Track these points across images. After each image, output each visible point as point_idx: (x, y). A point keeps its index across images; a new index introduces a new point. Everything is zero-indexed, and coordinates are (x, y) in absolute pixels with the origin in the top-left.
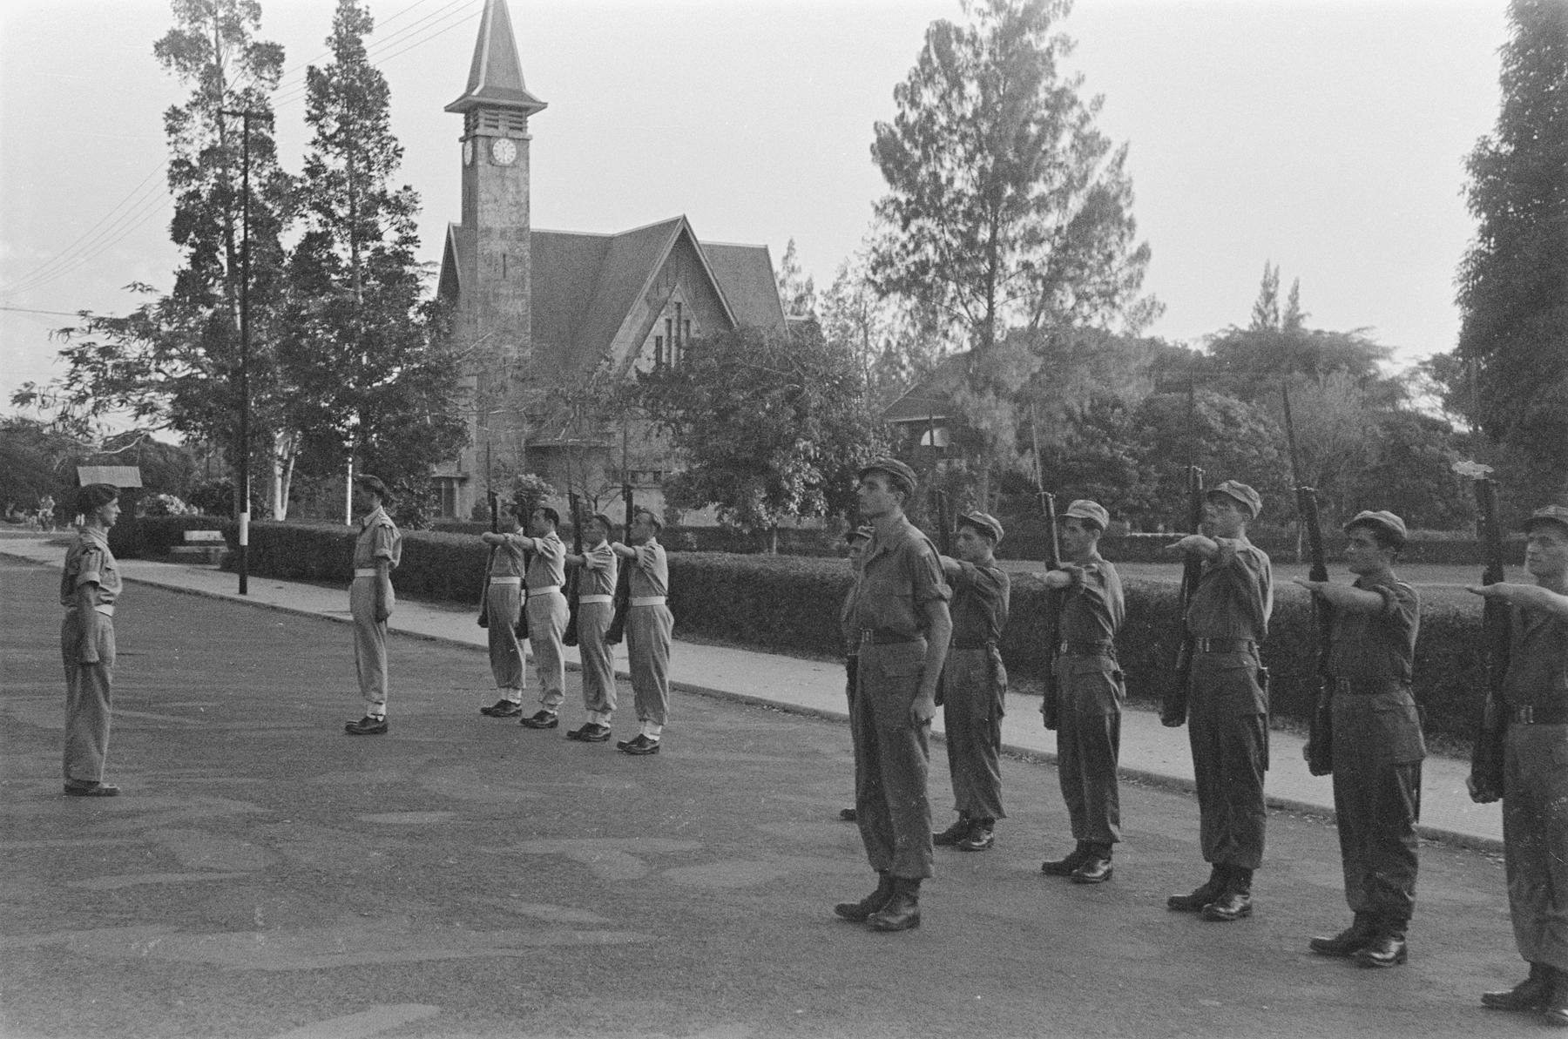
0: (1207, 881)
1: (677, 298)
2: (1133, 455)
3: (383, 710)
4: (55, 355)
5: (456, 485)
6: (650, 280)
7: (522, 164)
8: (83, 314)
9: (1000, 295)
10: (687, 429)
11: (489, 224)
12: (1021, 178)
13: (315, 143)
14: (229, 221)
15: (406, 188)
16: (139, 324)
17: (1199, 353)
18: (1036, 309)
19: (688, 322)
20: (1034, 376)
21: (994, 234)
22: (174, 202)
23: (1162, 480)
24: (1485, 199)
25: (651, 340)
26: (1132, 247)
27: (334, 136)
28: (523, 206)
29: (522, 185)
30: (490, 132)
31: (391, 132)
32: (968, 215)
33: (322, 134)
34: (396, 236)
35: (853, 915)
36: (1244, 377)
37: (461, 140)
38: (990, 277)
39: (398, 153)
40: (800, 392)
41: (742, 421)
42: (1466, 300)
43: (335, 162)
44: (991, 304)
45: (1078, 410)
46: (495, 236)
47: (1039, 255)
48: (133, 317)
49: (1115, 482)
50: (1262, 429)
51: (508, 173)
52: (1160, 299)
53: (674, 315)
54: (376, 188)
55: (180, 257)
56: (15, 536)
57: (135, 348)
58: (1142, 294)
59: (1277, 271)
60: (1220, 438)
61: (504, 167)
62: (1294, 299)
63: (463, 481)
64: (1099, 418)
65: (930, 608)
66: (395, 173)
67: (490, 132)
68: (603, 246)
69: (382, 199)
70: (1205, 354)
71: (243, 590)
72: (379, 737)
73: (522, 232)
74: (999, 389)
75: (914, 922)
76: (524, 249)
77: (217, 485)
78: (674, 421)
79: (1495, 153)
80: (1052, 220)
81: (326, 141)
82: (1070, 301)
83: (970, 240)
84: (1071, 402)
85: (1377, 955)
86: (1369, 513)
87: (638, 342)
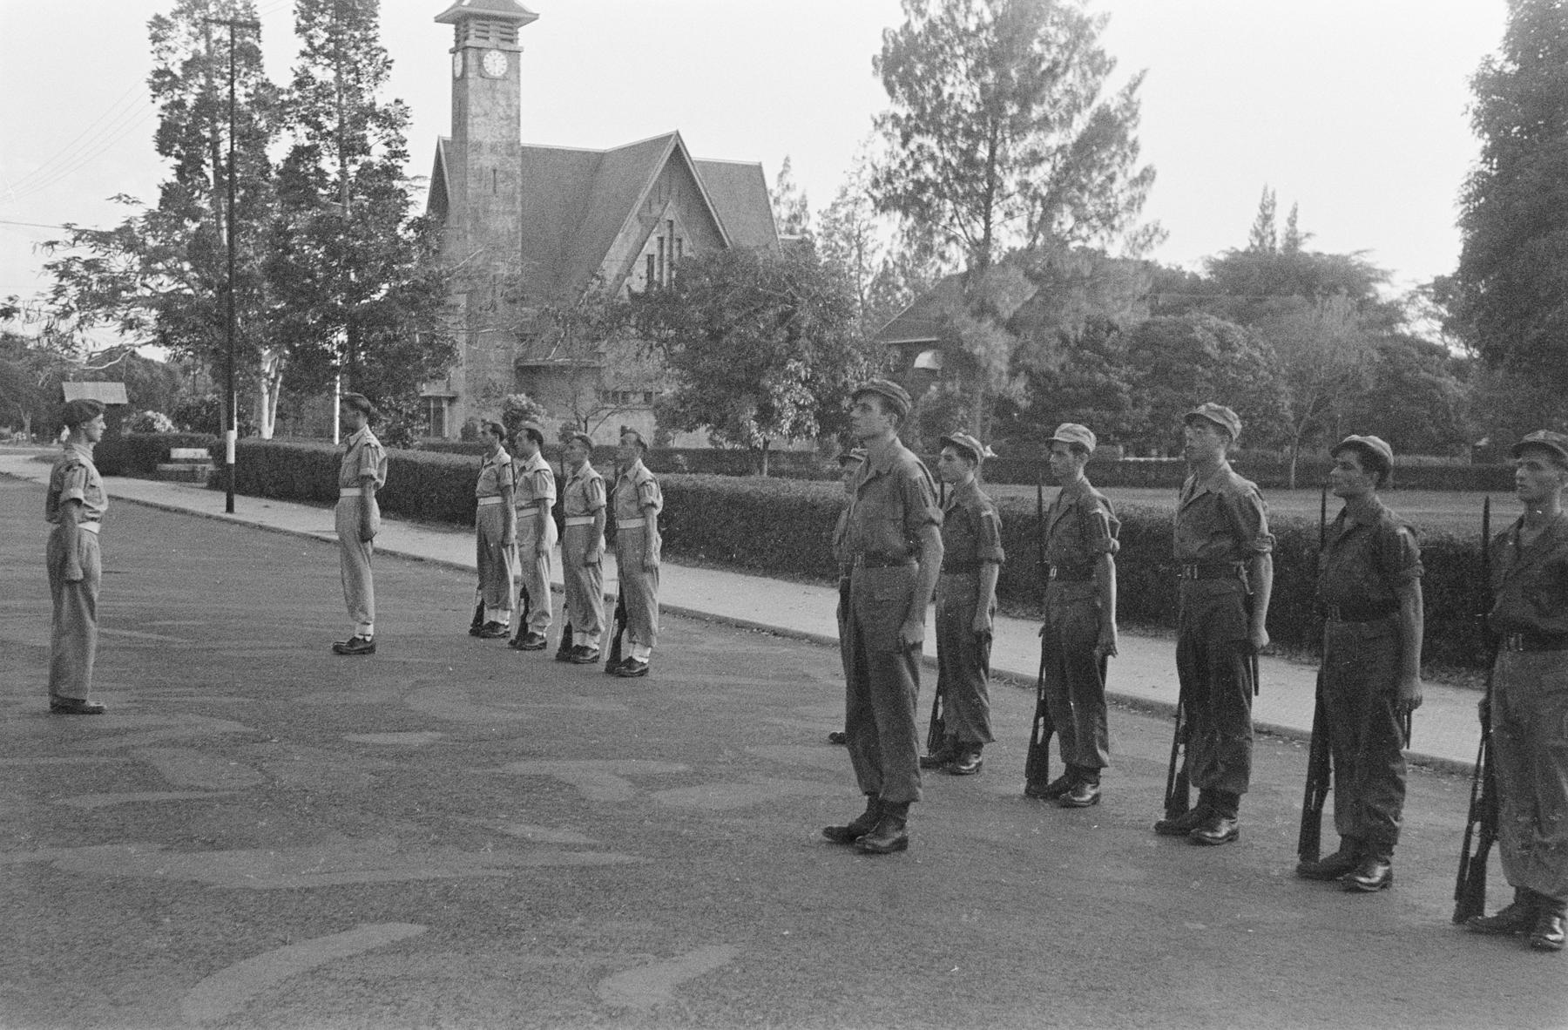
1: (669, 215)
3: (370, 630)
4: (40, 269)
5: (445, 405)
6: (642, 197)
8: (68, 226)
9: (997, 215)
10: (679, 348)
11: (479, 138)
12: (1026, 97)
14: (215, 132)
16: (126, 238)
19: (680, 240)
24: (1490, 119)
25: (642, 258)
26: (1135, 170)
27: (323, 47)
28: (514, 120)
29: (512, 97)
30: (480, 43)
33: (311, 45)
34: (385, 150)
37: (453, 52)
38: (988, 198)
39: (387, 64)
43: (323, 73)
44: (988, 223)
46: (486, 150)
47: (1040, 175)
49: (1109, 406)
50: (1257, 354)
51: (499, 86)
52: (1164, 226)
53: (666, 233)
55: (165, 170)
57: (121, 262)
61: (494, 80)
63: (452, 400)
64: (1093, 344)
67: (480, 43)
68: (594, 162)
69: (370, 113)
71: (230, 508)
73: (513, 147)
75: (901, 845)
76: (515, 166)
78: (666, 341)
81: (312, 53)
82: (1069, 222)
83: (968, 158)
84: (1067, 327)
85: (1363, 880)
86: (1356, 437)
87: (630, 261)
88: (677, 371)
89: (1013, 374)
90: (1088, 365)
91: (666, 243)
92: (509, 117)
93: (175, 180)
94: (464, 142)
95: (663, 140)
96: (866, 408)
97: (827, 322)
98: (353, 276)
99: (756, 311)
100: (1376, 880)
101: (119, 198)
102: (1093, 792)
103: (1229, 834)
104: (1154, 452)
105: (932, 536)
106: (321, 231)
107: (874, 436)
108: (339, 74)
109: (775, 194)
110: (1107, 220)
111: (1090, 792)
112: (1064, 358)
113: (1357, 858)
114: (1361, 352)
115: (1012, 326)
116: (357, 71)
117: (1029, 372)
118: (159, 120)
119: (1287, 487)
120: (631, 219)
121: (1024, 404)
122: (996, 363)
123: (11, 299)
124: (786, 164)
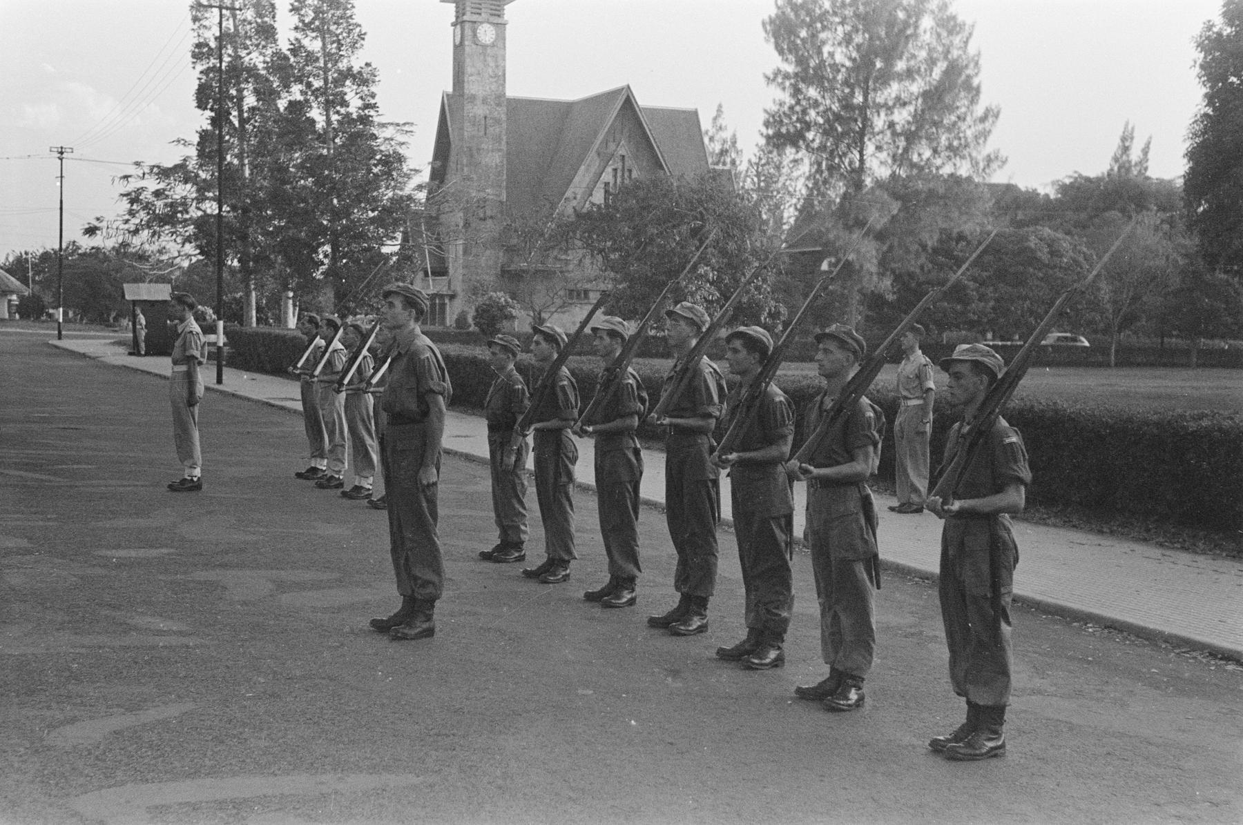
0: (675, 606)
1: (622, 151)
2: (975, 280)
3: (197, 472)
4: (116, 196)
5: (447, 301)
6: (601, 137)
7: (500, 44)
8: (138, 164)
9: (870, 148)
10: (614, 256)
11: (473, 92)
12: (890, 54)
13: (296, 28)
14: (240, 91)
15: (368, 65)
16: (180, 171)
17: (1047, 195)
18: (900, 159)
19: (630, 171)
20: (893, 217)
21: (866, 98)
22: (196, 74)
23: (997, 300)
24: (1213, 72)
25: (600, 185)
26: (979, 110)
27: (312, 22)
28: (501, 78)
29: (499, 61)
30: (475, 18)
31: (356, 20)
32: (846, 83)
33: (303, 21)
34: (360, 103)
35: (381, 627)
36: (1083, 216)
37: (454, 25)
38: (862, 134)
39: (362, 36)
40: (703, 226)
41: (656, 250)
42: (1192, 155)
43: (313, 44)
44: (861, 155)
45: (930, 243)
46: (479, 102)
47: (902, 117)
48: (176, 166)
49: (959, 301)
50: (1081, 259)
51: (489, 51)
52: (1003, 154)
53: (620, 165)
54: (343, 65)
55: (203, 120)
56: (84, 337)
57: (183, 191)
58: (988, 148)
59: (1133, 129)
60: (1047, 266)
61: (485, 47)
62: (1145, 151)
63: (452, 297)
64: (947, 250)
65: (429, 398)
66: (359, 53)
67: (475, 18)
68: (565, 109)
69: (348, 74)
70: (1052, 197)
71: (219, 381)
72: (193, 494)
73: (500, 97)
74: (860, 223)
75: (430, 632)
76: (501, 112)
77: (235, 299)
78: (603, 250)
79: (1219, 34)
80: (916, 87)
81: (305, 27)
82: (927, 153)
83: (847, 105)
84: (925, 236)
85: (756, 661)
86: (742, 328)
87: (589, 187)
88: (612, 275)
89: (881, 275)
90: (941, 267)
91: (619, 174)
92: (496, 76)
93: (209, 128)
94: (462, 95)
95: (611, 95)
96: (391, 305)
97: (729, 236)
98: (335, 201)
99: (674, 226)
100: (768, 661)
101: (179, 141)
102: (629, 596)
103: (699, 627)
104: (989, 336)
105: (437, 404)
106: (313, 166)
107: (399, 327)
108: (324, 44)
109: (710, 134)
110: (954, 151)
111: (627, 596)
112: (923, 260)
113: (758, 644)
114: (1167, 258)
115: (880, 236)
116: (338, 41)
117: (893, 272)
118: (197, 82)
119: (1109, 366)
120: (592, 154)
121: (890, 297)
122: (867, 266)
123: (98, 219)
124: (719, 110)
